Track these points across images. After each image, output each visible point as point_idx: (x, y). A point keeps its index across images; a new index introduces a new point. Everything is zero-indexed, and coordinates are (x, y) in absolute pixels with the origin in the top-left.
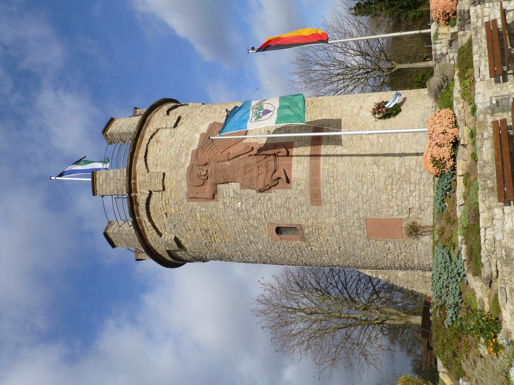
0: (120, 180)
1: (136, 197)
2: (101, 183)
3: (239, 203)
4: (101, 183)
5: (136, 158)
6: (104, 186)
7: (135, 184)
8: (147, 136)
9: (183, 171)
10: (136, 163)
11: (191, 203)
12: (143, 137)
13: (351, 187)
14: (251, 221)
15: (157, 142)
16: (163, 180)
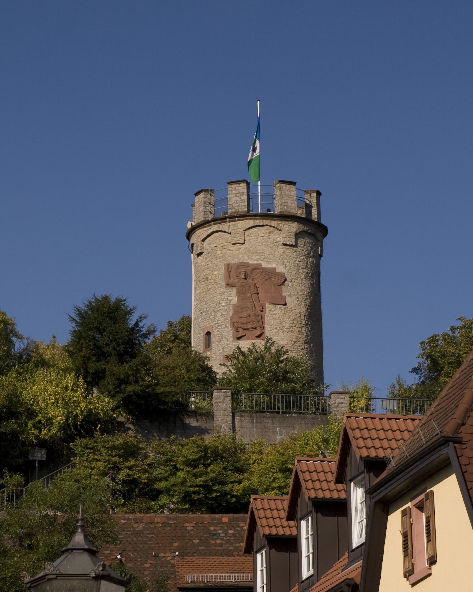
0: (239, 206)
1: (226, 222)
3: (224, 304)
4: (237, 188)
5: (255, 219)
6: (234, 192)
7: (235, 221)
8: (274, 223)
9: (246, 260)
10: (251, 219)
14: (213, 314)
15: (270, 233)
16: (239, 243)
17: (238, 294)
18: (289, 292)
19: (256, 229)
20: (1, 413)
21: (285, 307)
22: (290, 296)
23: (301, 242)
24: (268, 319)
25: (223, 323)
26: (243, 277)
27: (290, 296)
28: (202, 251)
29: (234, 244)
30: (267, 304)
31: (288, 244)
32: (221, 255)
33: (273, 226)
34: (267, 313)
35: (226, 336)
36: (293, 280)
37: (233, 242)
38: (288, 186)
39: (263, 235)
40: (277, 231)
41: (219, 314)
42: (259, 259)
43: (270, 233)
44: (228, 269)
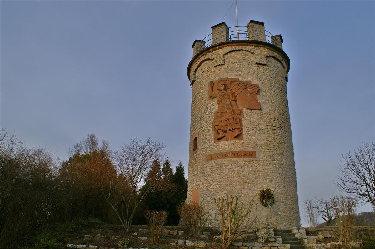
1: (210, 52)
2: (218, 30)
7: (216, 49)
8: (248, 48)
9: (226, 76)
10: (229, 46)
11: (208, 85)
12: (248, 46)
13: (215, 178)
15: (245, 55)
16: (220, 65)
17: (219, 102)
19: (233, 53)
21: (261, 111)
22: (264, 103)
25: (207, 128)
26: (222, 88)
28: (195, 79)
29: (216, 66)
30: (244, 109)
31: (261, 63)
32: (206, 77)
33: (247, 50)
34: (245, 117)
35: (209, 139)
36: (267, 91)
37: (215, 65)
38: (258, 25)
39: (239, 57)
40: (250, 54)
41: (204, 122)
42: (236, 75)
43: (245, 55)
44: (211, 85)
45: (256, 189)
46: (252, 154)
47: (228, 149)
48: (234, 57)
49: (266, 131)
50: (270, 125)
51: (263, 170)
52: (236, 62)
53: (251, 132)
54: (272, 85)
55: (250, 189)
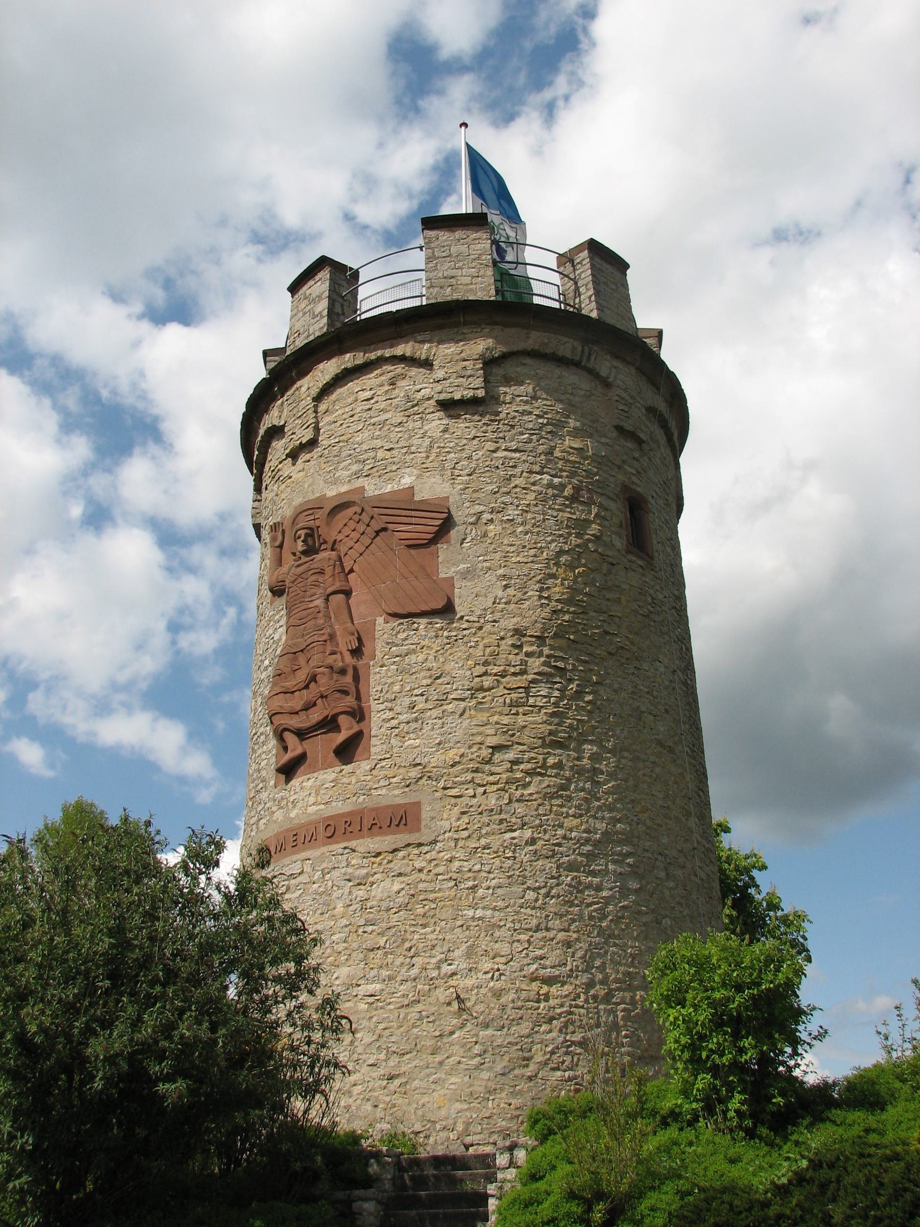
8: (404, 349)
18: (464, 561)
20: (587, 1222)
22: (466, 575)
23: (516, 397)
24: (380, 679)
27: (466, 575)
30: (380, 620)
31: (457, 397)
36: (486, 516)
39: (368, 394)
45: (414, 972)
46: (402, 818)
47: (315, 808)
48: (350, 400)
49: (474, 702)
50: (496, 669)
51: (452, 883)
52: (356, 418)
53: (403, 717)
54: (517, 481)
55: (390, 978)
